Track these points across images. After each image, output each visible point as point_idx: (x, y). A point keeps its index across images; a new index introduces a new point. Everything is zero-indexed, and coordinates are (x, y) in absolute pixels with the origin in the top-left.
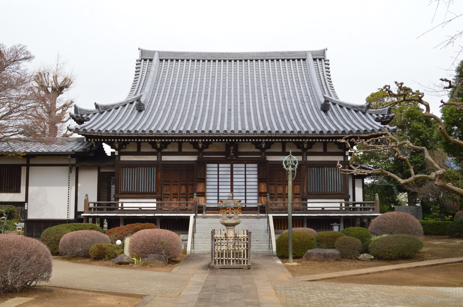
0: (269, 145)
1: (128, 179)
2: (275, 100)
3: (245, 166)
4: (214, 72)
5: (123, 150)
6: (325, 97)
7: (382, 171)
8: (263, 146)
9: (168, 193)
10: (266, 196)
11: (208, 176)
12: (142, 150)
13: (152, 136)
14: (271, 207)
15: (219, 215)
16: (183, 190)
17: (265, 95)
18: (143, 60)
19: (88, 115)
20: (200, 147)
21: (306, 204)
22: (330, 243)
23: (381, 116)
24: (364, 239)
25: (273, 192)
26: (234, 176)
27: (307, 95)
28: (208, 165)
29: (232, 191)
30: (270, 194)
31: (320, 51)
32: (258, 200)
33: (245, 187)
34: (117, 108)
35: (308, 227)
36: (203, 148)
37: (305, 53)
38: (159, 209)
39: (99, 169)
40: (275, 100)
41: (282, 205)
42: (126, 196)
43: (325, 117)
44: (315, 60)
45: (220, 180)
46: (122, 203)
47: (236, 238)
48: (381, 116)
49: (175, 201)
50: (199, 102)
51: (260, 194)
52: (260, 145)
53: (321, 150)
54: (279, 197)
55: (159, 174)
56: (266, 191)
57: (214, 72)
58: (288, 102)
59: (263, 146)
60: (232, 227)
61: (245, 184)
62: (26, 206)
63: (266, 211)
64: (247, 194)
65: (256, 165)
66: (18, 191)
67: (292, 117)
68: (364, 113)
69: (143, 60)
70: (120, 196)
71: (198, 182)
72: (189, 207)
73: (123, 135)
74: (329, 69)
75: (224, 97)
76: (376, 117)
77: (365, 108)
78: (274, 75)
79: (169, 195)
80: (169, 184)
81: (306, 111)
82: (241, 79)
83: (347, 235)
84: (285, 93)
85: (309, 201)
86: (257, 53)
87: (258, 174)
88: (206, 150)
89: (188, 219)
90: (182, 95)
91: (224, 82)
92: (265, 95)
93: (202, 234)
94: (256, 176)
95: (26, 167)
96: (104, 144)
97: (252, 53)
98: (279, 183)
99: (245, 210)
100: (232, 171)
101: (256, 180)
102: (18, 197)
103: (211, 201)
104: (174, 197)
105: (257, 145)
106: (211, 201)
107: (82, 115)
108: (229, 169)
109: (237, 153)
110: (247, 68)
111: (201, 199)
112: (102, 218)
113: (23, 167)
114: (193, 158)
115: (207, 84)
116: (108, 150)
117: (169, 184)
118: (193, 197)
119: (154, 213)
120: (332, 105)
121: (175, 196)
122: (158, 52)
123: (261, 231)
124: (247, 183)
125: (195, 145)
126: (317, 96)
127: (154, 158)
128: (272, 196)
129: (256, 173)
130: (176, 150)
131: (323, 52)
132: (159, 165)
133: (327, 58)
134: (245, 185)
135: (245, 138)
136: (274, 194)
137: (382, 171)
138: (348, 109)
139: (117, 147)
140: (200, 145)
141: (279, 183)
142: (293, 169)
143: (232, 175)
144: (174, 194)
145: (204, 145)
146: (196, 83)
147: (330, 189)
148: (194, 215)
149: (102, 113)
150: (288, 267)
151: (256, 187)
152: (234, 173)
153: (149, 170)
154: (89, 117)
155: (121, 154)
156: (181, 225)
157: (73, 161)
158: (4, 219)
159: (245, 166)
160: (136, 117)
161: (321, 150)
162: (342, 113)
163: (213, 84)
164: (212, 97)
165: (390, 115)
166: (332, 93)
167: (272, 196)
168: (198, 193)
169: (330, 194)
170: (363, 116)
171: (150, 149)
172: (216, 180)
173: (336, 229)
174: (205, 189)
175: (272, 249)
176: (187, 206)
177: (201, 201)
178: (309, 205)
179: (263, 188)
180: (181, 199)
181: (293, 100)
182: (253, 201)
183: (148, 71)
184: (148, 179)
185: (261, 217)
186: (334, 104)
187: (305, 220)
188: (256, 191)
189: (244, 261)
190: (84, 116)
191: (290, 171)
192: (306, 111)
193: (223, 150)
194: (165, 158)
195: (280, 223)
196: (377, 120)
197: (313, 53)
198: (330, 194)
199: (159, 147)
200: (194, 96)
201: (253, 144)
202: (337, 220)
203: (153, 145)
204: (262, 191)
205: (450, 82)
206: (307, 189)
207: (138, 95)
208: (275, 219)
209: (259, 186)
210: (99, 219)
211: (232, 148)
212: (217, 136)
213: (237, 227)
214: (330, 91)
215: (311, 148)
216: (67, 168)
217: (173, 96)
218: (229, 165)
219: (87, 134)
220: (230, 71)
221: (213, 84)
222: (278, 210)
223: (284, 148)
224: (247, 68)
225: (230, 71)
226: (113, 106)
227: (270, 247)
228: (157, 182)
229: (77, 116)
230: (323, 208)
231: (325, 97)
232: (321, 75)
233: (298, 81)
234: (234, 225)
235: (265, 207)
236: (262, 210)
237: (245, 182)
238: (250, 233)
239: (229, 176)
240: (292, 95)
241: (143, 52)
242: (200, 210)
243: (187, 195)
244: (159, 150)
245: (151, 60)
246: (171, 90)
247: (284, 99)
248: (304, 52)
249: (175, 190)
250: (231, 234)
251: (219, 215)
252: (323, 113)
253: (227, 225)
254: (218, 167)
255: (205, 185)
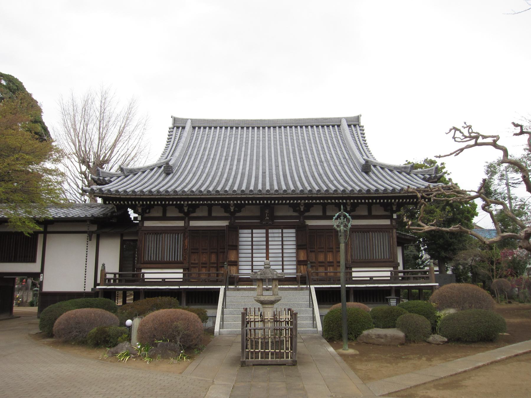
0: (308, 207)
1: (151, 248)
2: (312, 163)
3: (282, 231)
4: (247, 139)
5: (146, 215)
6: (364, 159)
7: (460, 228)
8: (302, 209)
9: (196, 262)
10: (306, 265)
11: (241, 243)
12: (168, 215)
13: (176, 197)
14: (312, 277)
15: (254, 287)
16: (213, 258)
17: (301, 158)
18: (175, 128)
19: (111, 178)
20: (232, 210)
21: (351, 273)
22: (388, 320)
23: (428, 176)
24: (429, 314)
25: (314, 260)
26: (270, 243)
27: (344, 158)
28: (241, 231)
29: (267, 257)
30: (311, 263)
31: (355, 117)
32: (297, 269)
33: (283, 255)
34: (144, 172)
35: (356, 300)
36: (235, 211)
37: (340, 120)
38: (185, 281)
39: (122, 236)
40: (312, 163)
41: (323, 274)
42: (148, 265)
43: (367, 178)
44: (349, 126)
45: (254, 247)
46: (144, 273)
47: (275, 320)
48: (428, 176)
49: (204, 271)
50: (232, 165)
51: (299, 263)
52: (298, 208)
53: (366, 213)
54: (320, 266)
55: (186, 241)
56: (306, 259)
57: (247, 139)
58: (325, 165)
59: (302, 209)
60: (270, 306)
61: (282, 251)
62: (41, 277)
63: (307, 281)
64: (285, 263)
65: (293, 231)
66: (34, 260)
67: (332, 178)
68: (409, 174)
69: (175, 128)
70: (142, 266)
71: (229, 249)
72: (220, 277)
73: (145, 197)
74: (364, 134)
75: (258, 161)
76: (422, 177)
77: (409, 169)
78: (309, 140)
79: (197, 264)
80: (198, 253)
81: (346, 172)
82: (275, 144)
83: (410, 312)
84: (322, 156)
85: (353, 269)
86: (291, 120)
87: (297, 241)
88: (238, 215)
89: (217, 291)
90: (214, 159)
91: (258, 147)
92: (301, 158)
93: (227, 316)
94: (294, 243)
95: (43, 235)
96: (129, 210)
97: (286, 120)
98: (319, 250)
99: (283, 280)
100: (267, 237)
101: (294, 247)
102: (34, 268)
103: (245, 270)
104: (202, 267)
105: (295, 207)
106: (245, 270)
107: (104, 178)
108: (264, 235)
109: (273, 217)
110: (280, 134)
111: (233, 269)
112: (125, 291)
113: (39, 235)
114: (224, 223)
115: (240, 149)
116: (132, 214)
117: (198, 253)
118: (223, 267)
119: (179, 286)
120: (372, 167)
121: (204, 265)
122: (191, 120)
123: (306, 309)
124: (285, 251)
125: (226, 207)
126: (356, 158)
127: (181, 224)
128: (313, 265)
129: (294, 239)
130: (206, 214)
131: (358, 118)
132: (186, 231)
133: (362, 124)
134: (283, 253)
135: (283, 199)
136: (314, 263)
137: (460, 228)
138: (391, 171)
139: (140, 210)
140: (232, 209)
141: (319, 250)
142: (345, 229)
143: (267, 241)
144: (202, 264)
145: (236, 209)
146: (229, 148)
147: (378, 256)
148: (224, 287)
149: (126, 176)
150: (341, 355)
151: (294, 255)
152: (270, 239)
153: (175, 235)
154: (112, 180)
155: (144, 219)
156: (211, 298)
157: (94, 228)
158: (37, 290)
159: (282, 231)
160: (163, 180)
161: (366, 213)
162: (384, 174)
163: (246, 149)
164: (245, 161)
165: (438, 175)
166: (369, 155)
167: (313, 265)
168: (229, 262)
169: (384, 262)
170: (408, 176)
171: (176, 213)
172: (250, 247)
173: (393, 302)
174: (238, 257)
175: (316, 327)
176: (217, 276)
177: (233, 271)
178: (354, 274)
179: (303, 257)
180: (211, 269)
181: (331, 163)
182: (291, 270)
183: (180, 138)
184: (171, 247)
185: (302, 289)
186: (375, 166)
187: (352, 292)
188: (295, 259)
189: (287, 353)
190: (106, 179)
191: (342, 231)
192: (346, 172)
193: (258, 214)
194: (193, 223)
195: (324, 297)
196: (424, 179)
197: (347, 119)
198: (384, 262)
199: (186, 211)
200: (226, 160)
201: (290, 206)
202: (387, 292)
203: (180, 208)
204: (302, 258)
205: (521, 127)
206: (351, 256)
207: (168, 158)
208: (317, 290)
209: (297, 253)
210: (121, 293)
211: (267, 211)
212: (250, 196)
213: (275, 306)
214: (367, 153)
215: (355, 211)
216: (86, 235)
217: (204, 160)
218: (264, 231)
219: (104, 195)
220: (264, 137)
221: (246, 149)
222: (320, 280)
223: (324, 211)
224: (280, 134)
225: (264, 137)
226: (139, 169)
227: (315, 326)
228: (184, 250)
229: (99, 179)
230: (371, 278)
231: (364, 159)
232: (357, 140)
233: (334, 145)
234: (272, 303)
235: (305, 277)
236: (302, 280)
237: (282, 249)
238: (296, 314)
239: (265, 243)
240: (329, 158)
241: (175, 120)
242: (234, 281)
243: (217, 265)
244: (187, 214)
245: (184, 128)
246: (203, 155)
247: (321, 162)
248: (338, 118)
249: (204, 258)
250: (269, 315)
251: (254, 287)
252: (364, 174)
253: (263, 303)
254: (252, 233)
255: (238, 253)
